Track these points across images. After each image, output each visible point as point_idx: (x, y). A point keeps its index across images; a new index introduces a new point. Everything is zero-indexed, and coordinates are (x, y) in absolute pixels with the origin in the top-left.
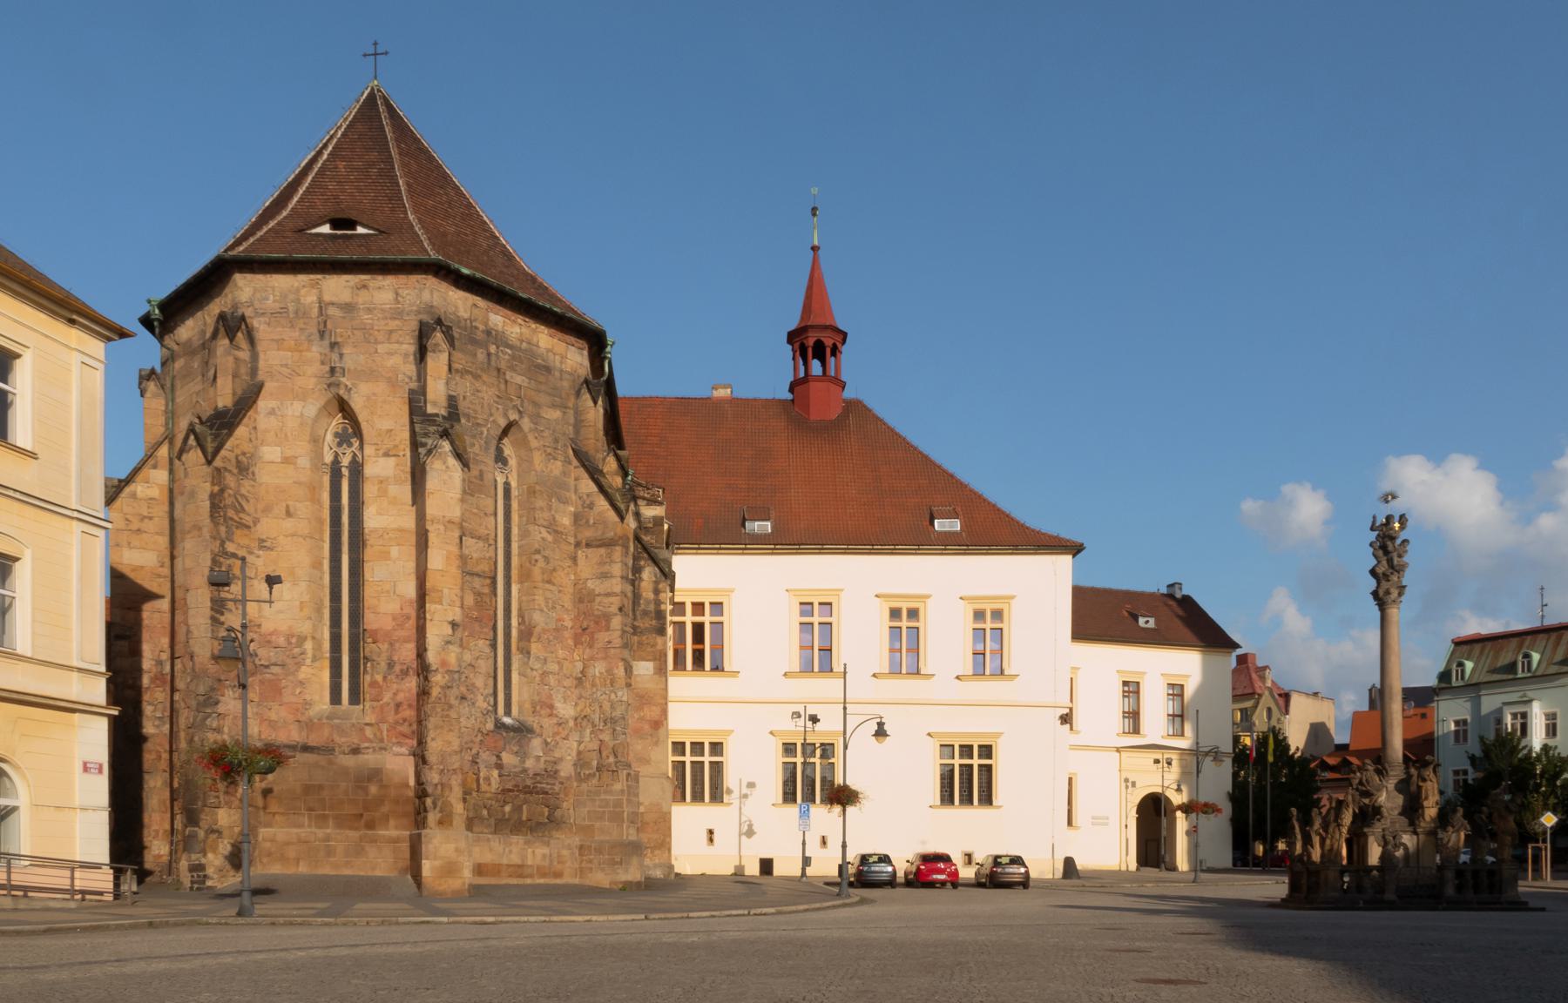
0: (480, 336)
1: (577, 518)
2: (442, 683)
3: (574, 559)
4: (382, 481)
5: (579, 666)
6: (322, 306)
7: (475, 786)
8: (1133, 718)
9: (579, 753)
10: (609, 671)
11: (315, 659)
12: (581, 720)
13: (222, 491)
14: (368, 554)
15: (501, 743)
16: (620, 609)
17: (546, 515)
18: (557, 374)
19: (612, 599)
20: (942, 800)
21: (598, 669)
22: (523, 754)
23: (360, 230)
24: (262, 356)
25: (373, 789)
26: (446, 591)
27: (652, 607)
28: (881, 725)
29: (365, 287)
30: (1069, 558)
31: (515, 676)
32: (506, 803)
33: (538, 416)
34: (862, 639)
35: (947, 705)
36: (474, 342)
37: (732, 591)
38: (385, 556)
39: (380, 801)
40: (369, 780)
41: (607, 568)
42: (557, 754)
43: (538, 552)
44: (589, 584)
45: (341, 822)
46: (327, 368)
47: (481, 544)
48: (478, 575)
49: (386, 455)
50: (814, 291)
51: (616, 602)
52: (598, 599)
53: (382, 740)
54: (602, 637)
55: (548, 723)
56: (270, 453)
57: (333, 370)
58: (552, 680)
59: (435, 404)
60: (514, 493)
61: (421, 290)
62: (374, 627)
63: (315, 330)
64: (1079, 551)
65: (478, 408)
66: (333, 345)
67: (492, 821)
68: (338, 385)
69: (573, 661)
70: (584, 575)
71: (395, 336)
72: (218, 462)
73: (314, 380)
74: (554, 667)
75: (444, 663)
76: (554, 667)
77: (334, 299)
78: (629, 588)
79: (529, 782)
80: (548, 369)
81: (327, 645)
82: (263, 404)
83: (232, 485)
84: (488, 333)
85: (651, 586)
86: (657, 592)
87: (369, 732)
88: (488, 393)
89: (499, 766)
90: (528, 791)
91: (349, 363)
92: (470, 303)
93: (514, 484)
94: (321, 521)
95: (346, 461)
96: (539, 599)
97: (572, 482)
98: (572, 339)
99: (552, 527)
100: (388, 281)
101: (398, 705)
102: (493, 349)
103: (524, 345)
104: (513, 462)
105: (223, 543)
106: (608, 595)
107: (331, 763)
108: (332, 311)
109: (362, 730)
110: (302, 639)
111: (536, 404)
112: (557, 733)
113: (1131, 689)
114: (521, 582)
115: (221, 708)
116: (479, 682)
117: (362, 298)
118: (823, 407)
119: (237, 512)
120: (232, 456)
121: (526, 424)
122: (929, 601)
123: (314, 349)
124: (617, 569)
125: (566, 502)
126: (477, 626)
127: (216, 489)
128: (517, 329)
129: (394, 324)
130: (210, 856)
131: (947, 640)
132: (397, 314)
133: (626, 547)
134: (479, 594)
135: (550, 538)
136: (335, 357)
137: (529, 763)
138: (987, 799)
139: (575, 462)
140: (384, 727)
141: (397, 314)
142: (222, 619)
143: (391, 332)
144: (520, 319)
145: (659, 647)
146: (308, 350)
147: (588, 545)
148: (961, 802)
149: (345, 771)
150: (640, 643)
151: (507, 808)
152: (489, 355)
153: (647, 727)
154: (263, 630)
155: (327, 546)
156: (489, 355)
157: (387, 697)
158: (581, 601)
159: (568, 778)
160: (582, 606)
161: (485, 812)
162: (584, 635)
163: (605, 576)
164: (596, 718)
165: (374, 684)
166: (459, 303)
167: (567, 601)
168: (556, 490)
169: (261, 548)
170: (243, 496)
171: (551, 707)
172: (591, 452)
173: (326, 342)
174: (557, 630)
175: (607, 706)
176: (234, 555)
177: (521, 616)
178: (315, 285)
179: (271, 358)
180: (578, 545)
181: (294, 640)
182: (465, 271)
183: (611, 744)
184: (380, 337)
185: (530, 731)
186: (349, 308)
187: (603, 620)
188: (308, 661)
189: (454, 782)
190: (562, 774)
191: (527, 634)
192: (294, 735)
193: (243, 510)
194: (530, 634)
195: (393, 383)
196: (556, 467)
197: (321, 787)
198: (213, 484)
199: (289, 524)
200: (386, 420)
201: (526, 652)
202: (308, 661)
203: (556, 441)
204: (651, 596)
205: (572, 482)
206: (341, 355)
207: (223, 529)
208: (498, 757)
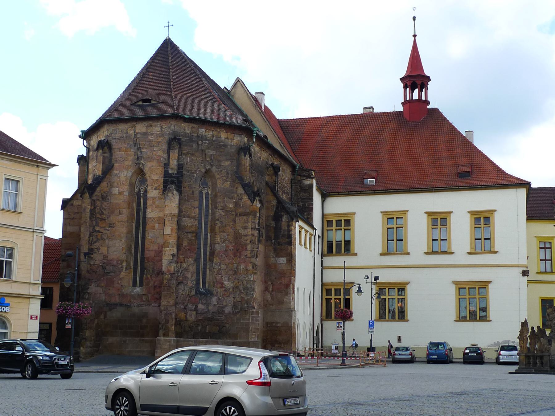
3: (235, 221)
4: (153, 199)
5: (235, 265)
9: (234, 302)
10: (246, 268)
11: (126, 269)
12: (235, 288)
13: (95, 208)
14: (148, 227)
16: (251, 242)
19: (248, 237)
21: (242, 267)
22: (208, 304)
23: (153, 102)
25: (144, 321)
26: (171, 242)
27: (286, 233)
28: (359, 288)
29: (151, 126)
31: (208, 271)
33: (220, 165)
34: (417, 232)
37: (355, 213)
38: (153, 228)
42: (224, 304)
43: (218, 220)
44: (240, 231)
46: (136, 157)
47: (192, 220)
49: (156, 189)
50: (415, 59)
52: (243, 237)
56: (116, 191)
57: (138, 157)
58: (223, 272)
59: (172, 169)
62: (148, 256)
66: (139, 149)
68: (139, 163)
69: (233, 264)
70: (238, 228)
71: (161, 144)
72: (94, 198)
73: (131, 162)
74: (224, 267)
75: (169, 271)
76: (224, 267)
77: (140, 131)
80: (225, 146)
81: (132, 263)
83: (99, 205)
84: (198, 137)
85: (286, 224)
88: (197, 160)
91: (144, 155)
92: (190, 127)
93: (210, 193)
95: (142, 191)
96: (218, 239)
99: (225, 209)
100: (159, 124)
101: (155, 287)
106: (246, 236)
110: (122, 262)
111: (219, 161)
112: (225, 295)
114: (211, 232)
115: (90, 291)
116: (189, 275)
117: (150, 130)
119: (101, 215)
120: (99, 194)
121: (214, 169)
123: (132, 150)
127: (93, 207)
129: (160, 139)
130: (82, 348)
131: (461, 231)
132: (162, 135)
134: (191, 240)
135: (223, 214)
136: (139, 153)
137: (210, 308)
140: (150, 296)
141: (162, 135)
142: (92, 256)
143: (159, 142)
145: (289, 251)
147: (240, 215)
151: (200, 328)
152: (198, 145)
153: (283, 287)
155: (134, 224)
156: (198, 145)
157: (151, 284)
158: (237, 238)
163: (246, 228)
164: (241, 287)
165: (147, 278)
166: (186, 128)
167: (231, 239)
169: (109, 227)
170: (103, 208)
171: (222, 283)
173: (136, 147)
174: (226, 251)
176: (99, 231)
177: (211, 246)
178: (133, 126)
180: (236, 215)
181: (119, 262)
182: (187, 117)
183: (246, 298)
186: (144, 134)
188: (124, 270)
190: (226, 312)
191: (212, 253)
192: (117, 299)
193: (103, 214)
195: (159, 162)
198: (91, 206)
199: (120, 218)
200: (155, 174)
201: (212, 261)
202: (124, 270)
203: (228, 174)
206: (141, 152)
207: (94, 222)
208: (197, 306)
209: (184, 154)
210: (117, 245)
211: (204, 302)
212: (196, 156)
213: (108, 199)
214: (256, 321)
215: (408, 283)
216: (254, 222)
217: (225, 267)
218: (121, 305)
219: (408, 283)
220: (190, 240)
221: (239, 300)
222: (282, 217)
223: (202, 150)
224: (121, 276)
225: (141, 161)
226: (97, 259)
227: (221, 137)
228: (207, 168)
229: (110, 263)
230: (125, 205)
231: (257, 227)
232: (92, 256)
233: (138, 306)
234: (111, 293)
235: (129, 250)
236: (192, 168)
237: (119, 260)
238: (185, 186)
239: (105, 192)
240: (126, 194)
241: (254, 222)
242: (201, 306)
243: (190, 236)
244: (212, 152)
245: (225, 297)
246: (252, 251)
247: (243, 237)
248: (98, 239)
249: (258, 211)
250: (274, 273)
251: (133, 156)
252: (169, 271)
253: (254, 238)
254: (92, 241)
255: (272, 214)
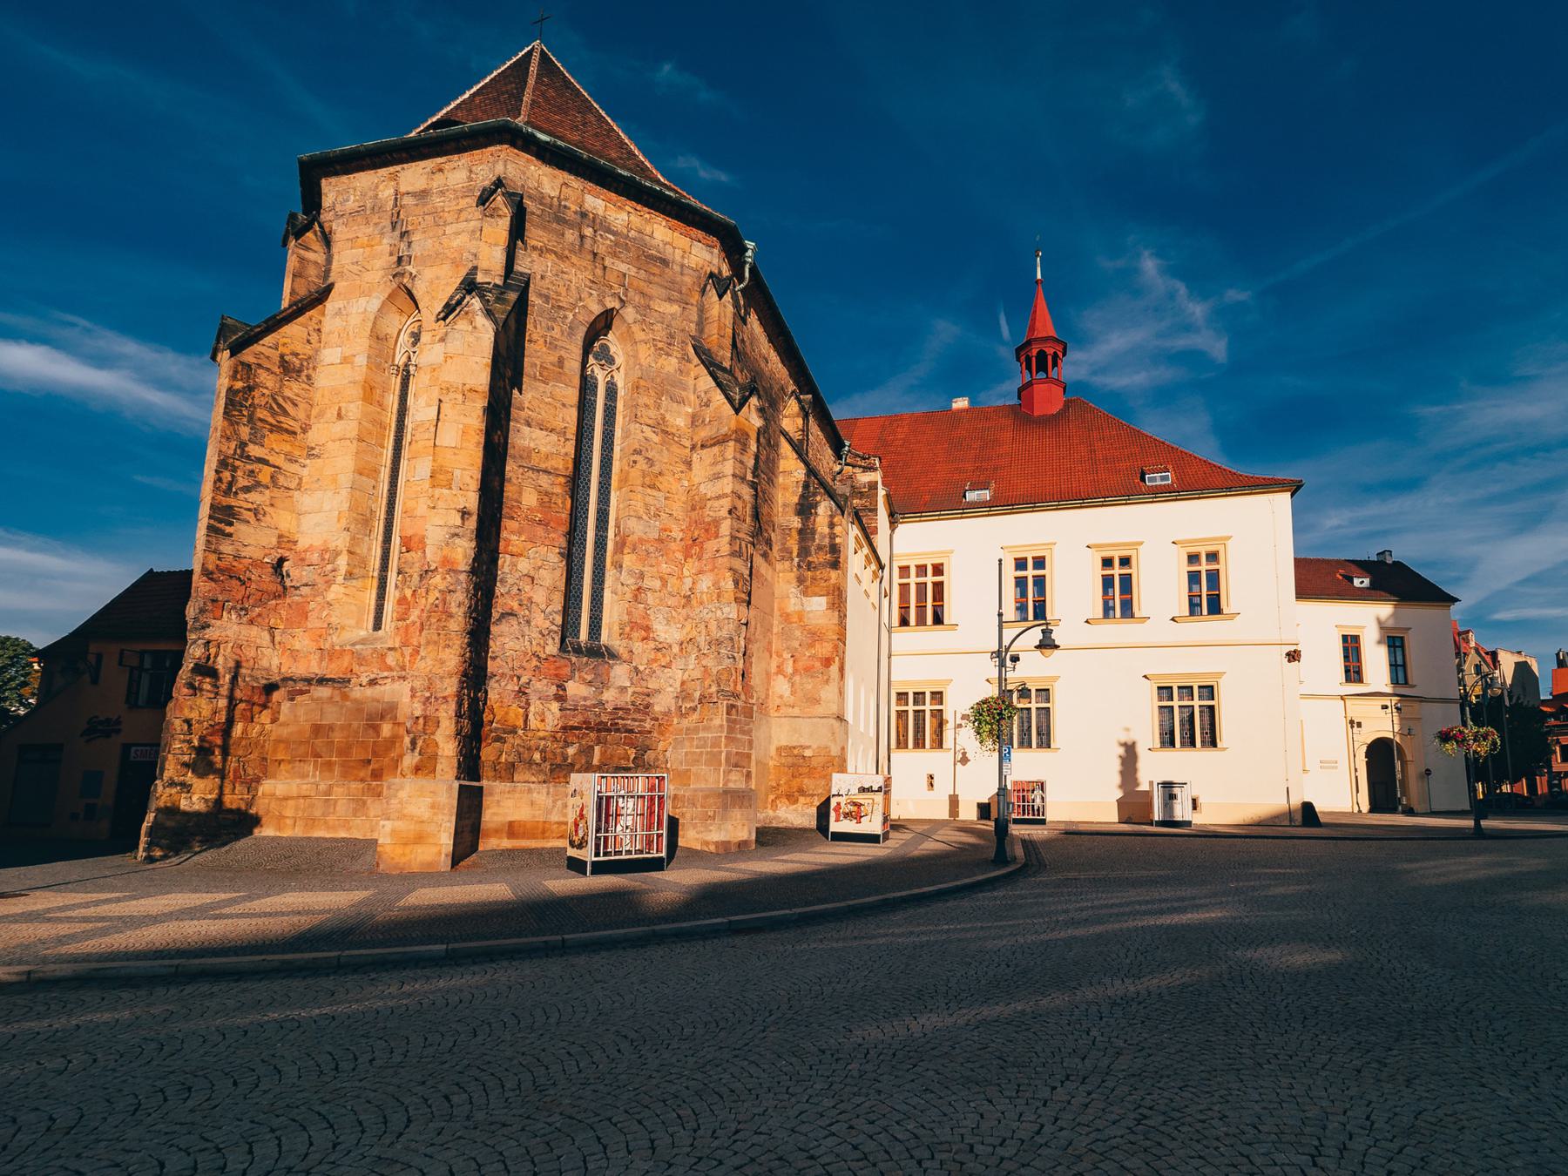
0: (570, 215)
1: (694, 420)
2: (442, 587)
3: (689, 464)
5: (688, 582)
6: (397, 195)
7: (521, 723)
8: (1353, 672)
9: (683, 683)
10: (716, 584)
11: (350, 575)
13: (250, 389)
15: (567, 670)
16: (730, 512)
17: (652, 413)
18: (677, 268)
20: (1163, 744)
22: (602, 683)
24: (336, 257)
25: (386, 729)
26: (457, 473)
27: (827, 541)
29: (441, 170)
30: (1286, 497)
32: (567, 744)
35: (1166, 641)
36: (561, 221)
39: (393, 741)
40: (382, 718)
41: (718, 468)
42: (652, 685)
44: (702, 489)
45: (347, 772)
46: (395, 258)
47: (554, 437)
48: (546, 471)
51: (726, 503)
52: (709, 504)
53: (403, 668)
54: (711, 546)
55: (638, 647)
57: (400, 259)
58: (651, 598)
59: (487, 272)
60: (621, 393)
61: (495, 163)
63: (388, 224)
64: (1299, 488)
65: (563, 290)
66: (403, 235)
67: (547, 765)
70: (696, 480)
71: (464, 215)
73: (381, 273)
77: (410, 189)
78: (747, 493)
79: (604, 718)
80: (665, 262)
82: (331, 305)
83: (269, 384)
84: (584, 215)
86: (832, 525)
87: (391, 659)
89: (560, 698)
90: (601, 728)
93: (620, 384)
94: (382, 426)
97: (691, 382)
98: (700, 234)
99: (660, 427)
102: (588, 232)
103: (632, 234)
104: (619, 360)
105: (243, 445)
106: (718, 498)
107: (345, 697)
108: (407, 200)
109: (383, 656)
112: (655, 660)
113: (1351, 646)
116: (539, 596)
117: (439, 180)
118: (1048, 401)
119: (274, 414)
122: (1141, 548)
124: (728, 468)
125: (681, 402)
126: (540, 531)
128: (624, 216)
131: (1161, 586)
133: (744, 448)
135: (656, 439)
136: (403, 246)
137: (609, 696)
138: (1212, 741)
139: (696, 360)
144: (630, 205)
146: (380, 243)
147: (703, 446)
148: (1183, 745)
149: (359, 706)
150: (813, 579)
151: (571, 751)
152: (582, 237)
153: (818, 664)
154: (300, 547)
156: (582, 237)
158: (693, 509)
159: (667, 713)
160: (694, 515)
161: (537, 756)
162: (693, 546)
163: (717, 477)
164: (702, 640)
166: (544, 181)
167: (678, 509)
168: (666, 388)
169: (309, 456)
171: (647, 629)
172: (714, 349)
173: (397, 233)
174: (660, 540)
175: (713, 626)
177: (617, 526)
178: (394, 177)
179: (344, 256)
180: (693, 448)
184: (449, 220)
185: (613, 656)
186: (423, 194)
187: (711, 529)
188: (340, 579)
189: (442, 715)
190: (657, 708)
193: (285, 413)
194: (624, 544)
196: (671, 364)
197: (331, 728)
199: (338, 428)
202: (340, 579)
203: (671, 336)
204: (826, 530)
205: (691, 382)
206: (410, 244)
208: (561, 687)
209: (534, 248)
210: (326, 507)
211: (589, 678)
212: (574, 265)
213: (309, 377)
214: (743, 732)
215: (1056, 678)
216: (741, 462)
217: (657, 584)
218: (322, 681)
219: (1056, 678)
220: (545, 496)
221: (697, 674)
222: (816, 505)
223: (595, 255)
224: (330, 596)
225: (409, 268)
226: (252, 540)
227: (651, 236)
228: (609, 306)
229: (303, 560)
230: (357, 392)
231: (749, 477)
232: (228, 529)
233: (373, 682)
234: (297, 646)
235: (366, 522)
236: (559, 294)
237: (326, 550)
238: (535, 337)
239: (296, 355)
240: (361, 360)
241: (741, 462)
242: (574, 689)
243: (544, 481)
244: (623, 267)
245: (655, 666)
246: (733, 538)
247: (709, 504)
248: (258, 484)
249: (753, 436)
250: (798, 633)
251: (386, 257)
252: (445, 561)
253: (739, 505)
254: (231, 484)
255: (796, 499)
